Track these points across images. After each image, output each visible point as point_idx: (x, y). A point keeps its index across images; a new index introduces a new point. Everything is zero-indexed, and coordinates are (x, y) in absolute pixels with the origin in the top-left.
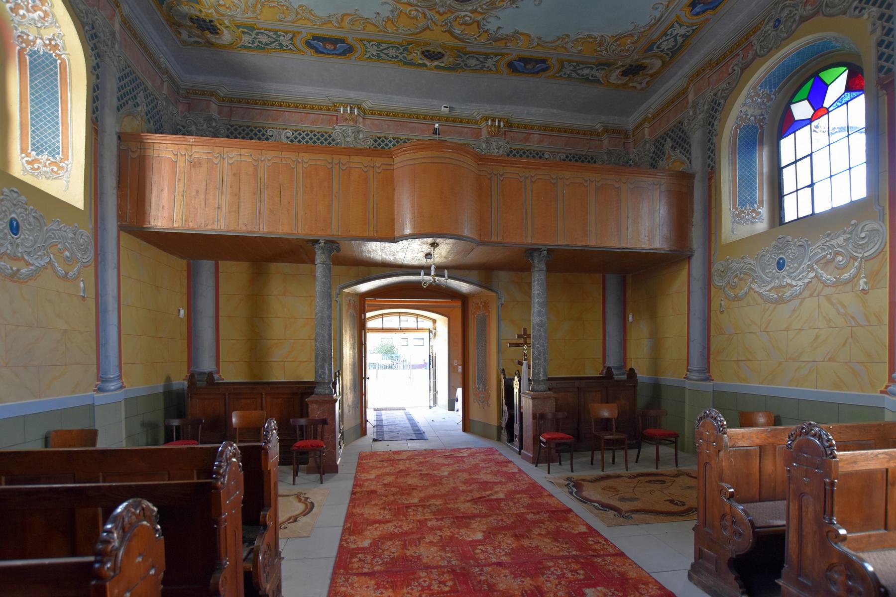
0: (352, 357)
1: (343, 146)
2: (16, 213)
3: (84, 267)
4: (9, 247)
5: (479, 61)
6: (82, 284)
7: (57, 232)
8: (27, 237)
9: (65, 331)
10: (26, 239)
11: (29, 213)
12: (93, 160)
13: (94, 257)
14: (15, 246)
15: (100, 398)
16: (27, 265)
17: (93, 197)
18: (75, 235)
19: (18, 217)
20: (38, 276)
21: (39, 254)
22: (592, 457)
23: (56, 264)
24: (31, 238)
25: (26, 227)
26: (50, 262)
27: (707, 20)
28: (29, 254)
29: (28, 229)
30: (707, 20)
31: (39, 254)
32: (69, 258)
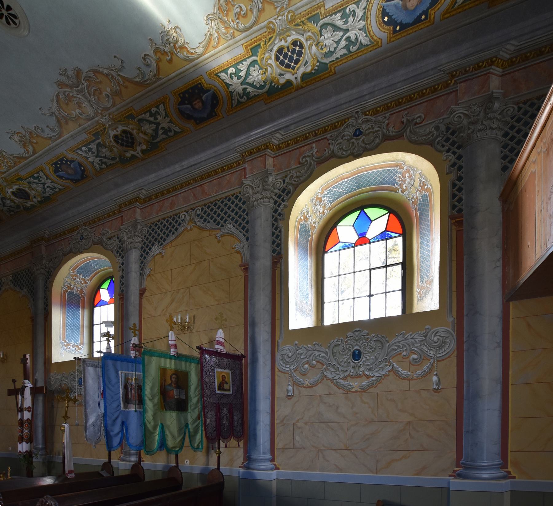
0: (434, 253)
1: (34, 460)
2: (358, 345)
3: (438, 361)
4: (352, 370)
5: (451, 93)
6: (435, 378)
7: (402, 342)
8: (368, 358)
9: (409, 423)
10: (367, 359)
11: (370, 340)
12: (120, 317)
13: (455, 347)
14: (357, 368)
15: (456, 484)
16: (368, 378)
17: (454, 288)
18: (425, 336)
19: (360, 347)
20: (379, 383)
21: (380, 366)
22: (386, 244)
23: (400, 369)
24: (372, 357)
25: (368, 351)
26: (393, 370)
27: (147, 420)
28: (370, 370)
29: (369, 352)
30: (147, 420)
31: (380, 366)
32: (416, 359)
